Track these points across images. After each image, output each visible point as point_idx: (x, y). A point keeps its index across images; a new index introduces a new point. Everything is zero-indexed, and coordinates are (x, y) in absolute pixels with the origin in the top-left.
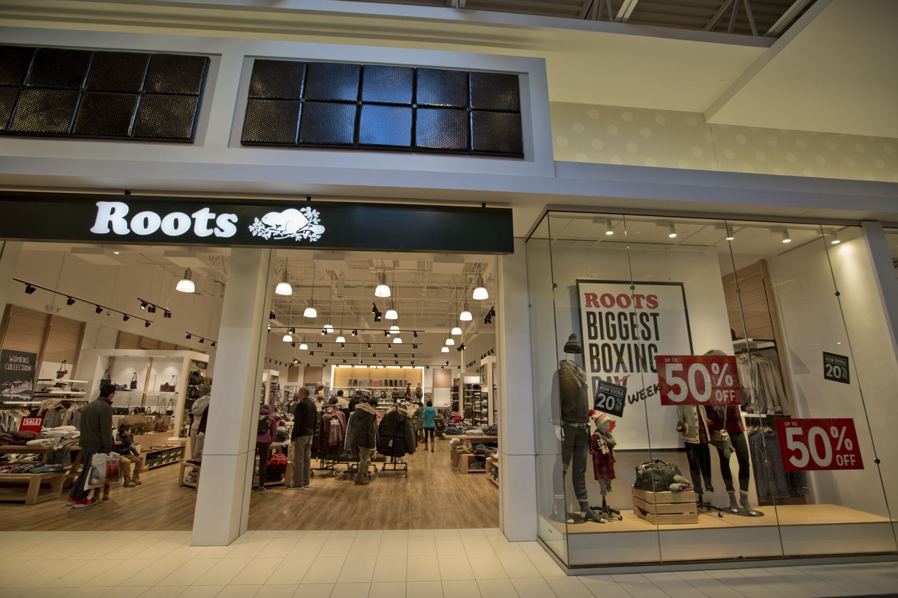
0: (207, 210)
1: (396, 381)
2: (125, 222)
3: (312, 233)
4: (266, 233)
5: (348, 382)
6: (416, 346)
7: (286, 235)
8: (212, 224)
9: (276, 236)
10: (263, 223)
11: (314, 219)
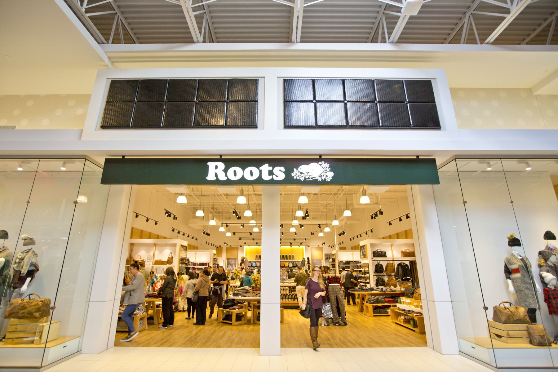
0: (267, 165)
1: (286, 256)
2: (224, 173)
3: (327, 176)
4: (302, 177)
5: (255, 257)
6: (313, 233)
7: (313, 178)
8: (271, 173)
9: (307, 179)
10: (299, 171)
11: (327, 168)
